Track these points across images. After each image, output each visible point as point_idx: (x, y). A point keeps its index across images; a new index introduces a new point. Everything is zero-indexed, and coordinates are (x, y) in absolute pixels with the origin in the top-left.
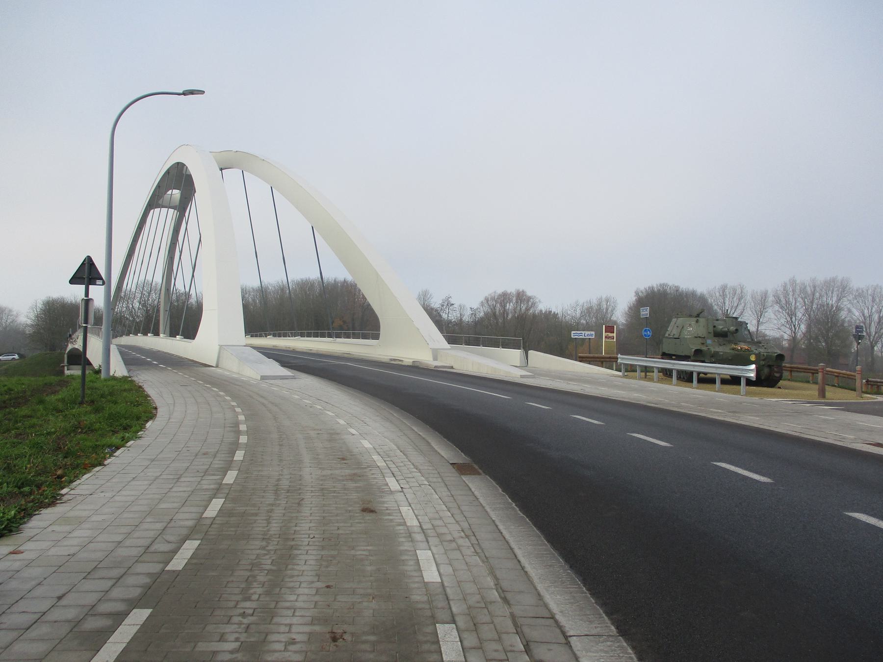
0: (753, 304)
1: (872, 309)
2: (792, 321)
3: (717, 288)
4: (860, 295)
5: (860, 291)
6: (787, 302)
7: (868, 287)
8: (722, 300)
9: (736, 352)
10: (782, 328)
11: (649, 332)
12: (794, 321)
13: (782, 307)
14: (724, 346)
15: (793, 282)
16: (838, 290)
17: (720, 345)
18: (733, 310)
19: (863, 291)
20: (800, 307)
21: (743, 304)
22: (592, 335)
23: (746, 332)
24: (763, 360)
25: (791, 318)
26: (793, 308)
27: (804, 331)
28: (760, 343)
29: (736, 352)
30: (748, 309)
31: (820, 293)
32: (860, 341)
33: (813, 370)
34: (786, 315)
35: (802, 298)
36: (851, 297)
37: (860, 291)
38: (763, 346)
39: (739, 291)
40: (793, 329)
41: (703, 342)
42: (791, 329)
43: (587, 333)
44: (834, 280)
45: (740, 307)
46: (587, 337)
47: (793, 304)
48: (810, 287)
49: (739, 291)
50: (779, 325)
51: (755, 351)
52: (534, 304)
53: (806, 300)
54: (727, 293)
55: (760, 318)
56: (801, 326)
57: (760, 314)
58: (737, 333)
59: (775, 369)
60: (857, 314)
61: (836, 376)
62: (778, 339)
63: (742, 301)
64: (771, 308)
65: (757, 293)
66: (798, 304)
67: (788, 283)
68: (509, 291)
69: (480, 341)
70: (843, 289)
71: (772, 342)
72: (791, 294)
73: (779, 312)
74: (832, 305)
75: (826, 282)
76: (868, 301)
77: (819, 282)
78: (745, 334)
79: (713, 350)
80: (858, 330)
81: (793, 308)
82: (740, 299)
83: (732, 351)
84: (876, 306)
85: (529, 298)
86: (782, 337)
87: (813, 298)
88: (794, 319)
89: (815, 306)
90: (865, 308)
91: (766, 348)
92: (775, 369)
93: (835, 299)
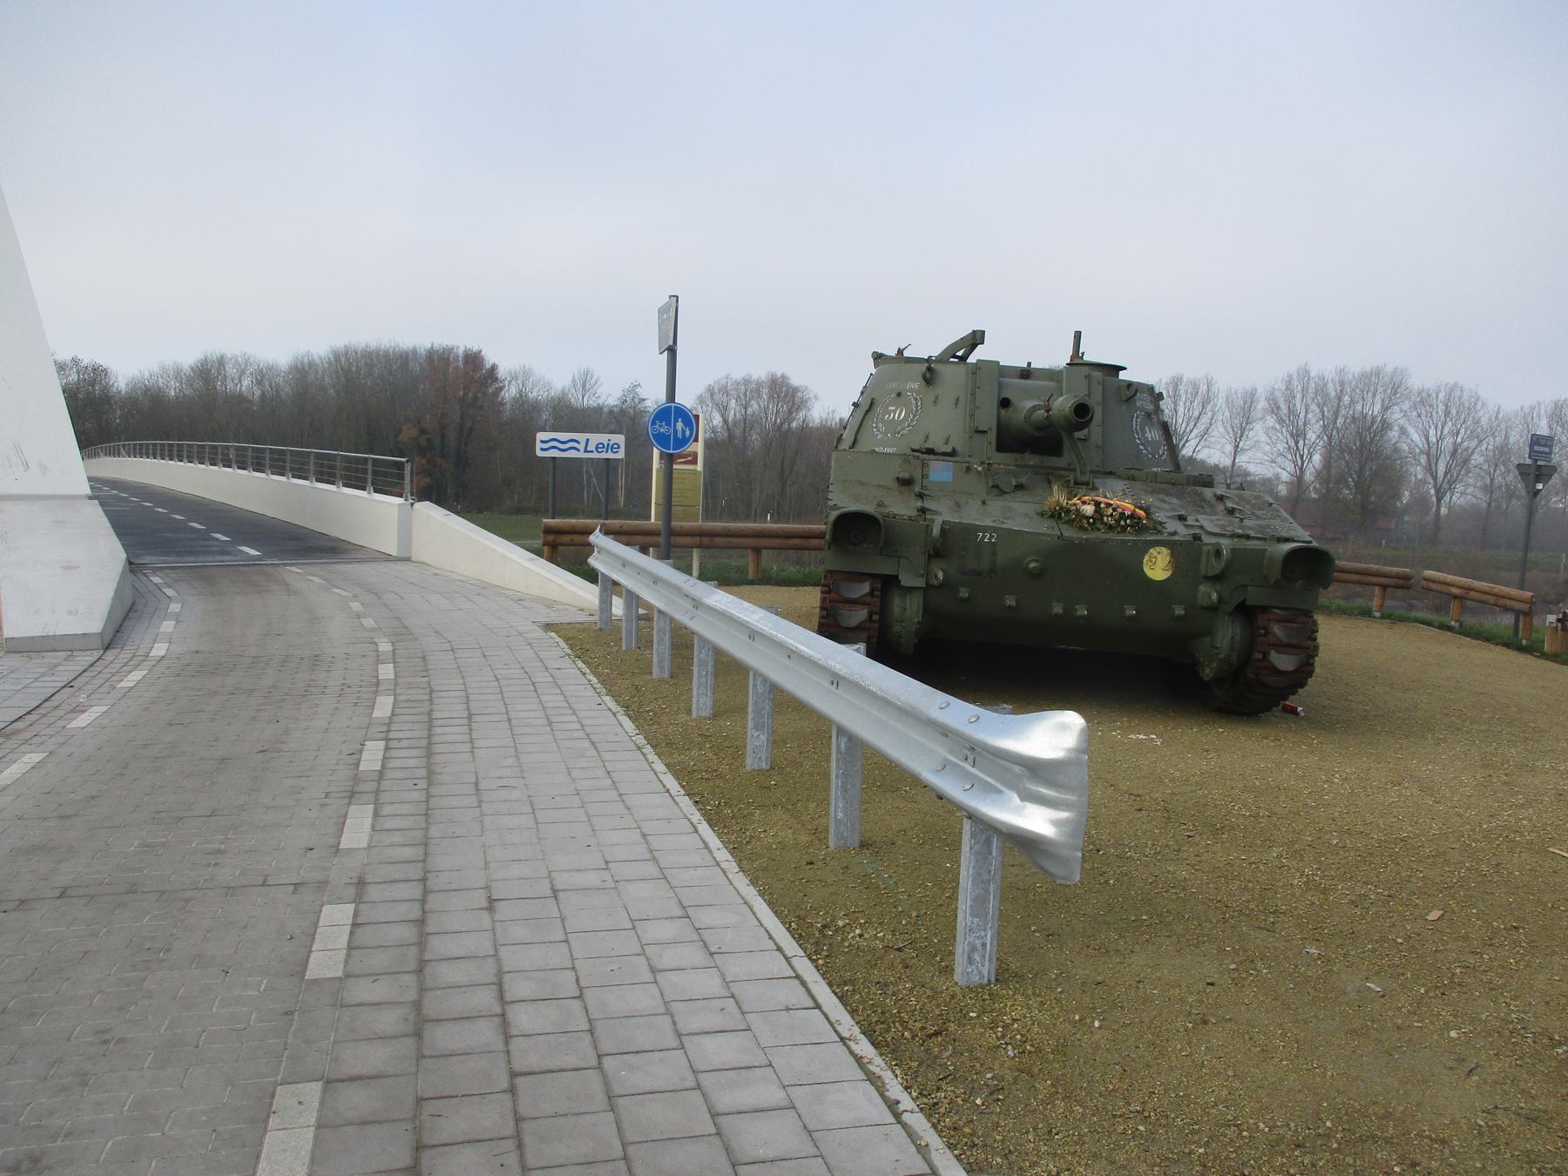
0: (1227, 414)
1: (1443, 428)
2: (1298, 448)
3: (1163, 382)
4: (1424, 400)
5: (1424, 394)
6: (1292, 412)
7: (1439, 387)
8: (1173, 406)
9: (1069, 532)
10: (1279, 460)
11: (680, 425)
12: (1301, 448)
13: (1281, 421)
14: (1019, 494)
15: (1304, 374)
16: (1385, 391)
17: (998, 490)
18: (1191, 425)
19: (1429, 395)
20: (1313, 421)
21: (1209, 415)
22: (613, 447)
23: (1153, 434)
24: (1216, 579)
25: (1297, 443)
26: (1301, 423)
27: (1317, 467)
28: (1209, 483)
29: (1069, 532)
30: (1219, 423)
31: (1350, 397)
32: (1540, 486)
33: (1386, 576)
34: (1288, 437)
35: (1318, 405)
36: (1406, 405)
37: (1424, 394)
38: (1221, 498)
39: (1203, 388)
40: (1299, 462)
41: (905, 475)
42: (1295, 462)
43: (596, 439)
44: (1378, 372)
45: (1204, 420)
46: (595, 455)
47: (1302, 415)
48: (1334, 383)
49: (1203, 388)
50: (1273, 454)
51: (1172, 526)
52: (803, 404)
53: (1325, 409)
54: (1182, 392)
55: (1240, 440)
56: (1314, 457)
57: (1240, 433)
58: (1086, 425)
59: (1277, 629)
60: (1415, 437)
61: (1455, 597)
62: (1269, 480)
63: (1209, 407)
64: (1261, 422)
65: (1236, 392)
66: (1310, 416)
67: (1295, 376)
68: (755, 377)
69: (365, 471)
70: (1395, 389)
71: (1258, 485)
72: (1299, 396)
73: (1275, 429)
74: (1374, 418)
75: (1362, 375)
76: (1437, 413)
77: (1351, 377)
78: (1146, 443)
79: (943, 513)
80: (1536, 448)
81: (1301, 423)
82: (1204, 405)
83: (1045, 528)
84: (1450, 424)
85: (796, 390)
86: (1277, 477)
87: (1339, 406)
88: (1301, 443)
89: (1340, 421)
90: (1430, 427)
91: (1231, 512)
92: (1277, 629)
93: (1377, 408)
